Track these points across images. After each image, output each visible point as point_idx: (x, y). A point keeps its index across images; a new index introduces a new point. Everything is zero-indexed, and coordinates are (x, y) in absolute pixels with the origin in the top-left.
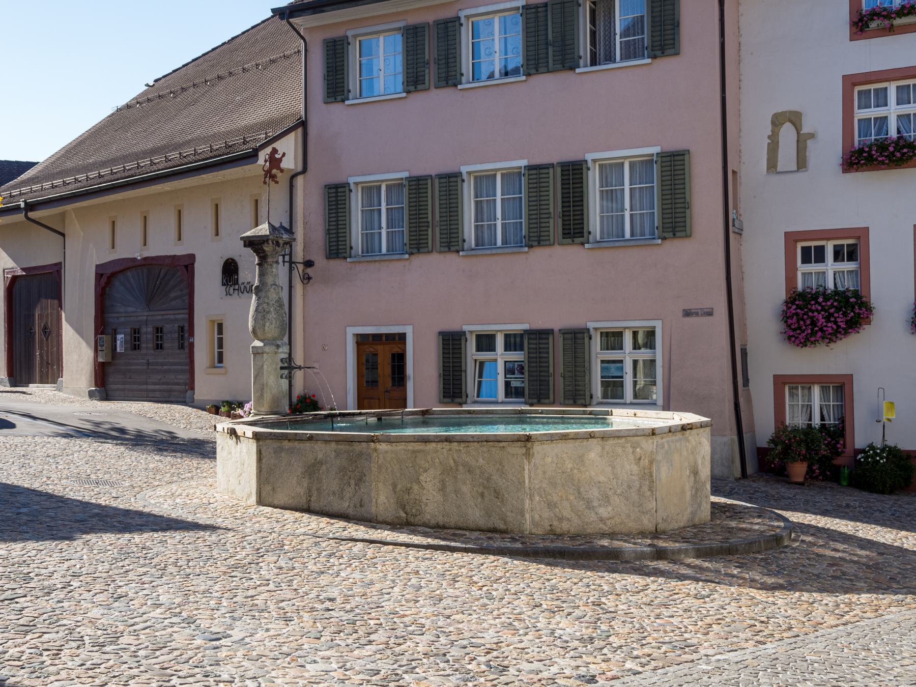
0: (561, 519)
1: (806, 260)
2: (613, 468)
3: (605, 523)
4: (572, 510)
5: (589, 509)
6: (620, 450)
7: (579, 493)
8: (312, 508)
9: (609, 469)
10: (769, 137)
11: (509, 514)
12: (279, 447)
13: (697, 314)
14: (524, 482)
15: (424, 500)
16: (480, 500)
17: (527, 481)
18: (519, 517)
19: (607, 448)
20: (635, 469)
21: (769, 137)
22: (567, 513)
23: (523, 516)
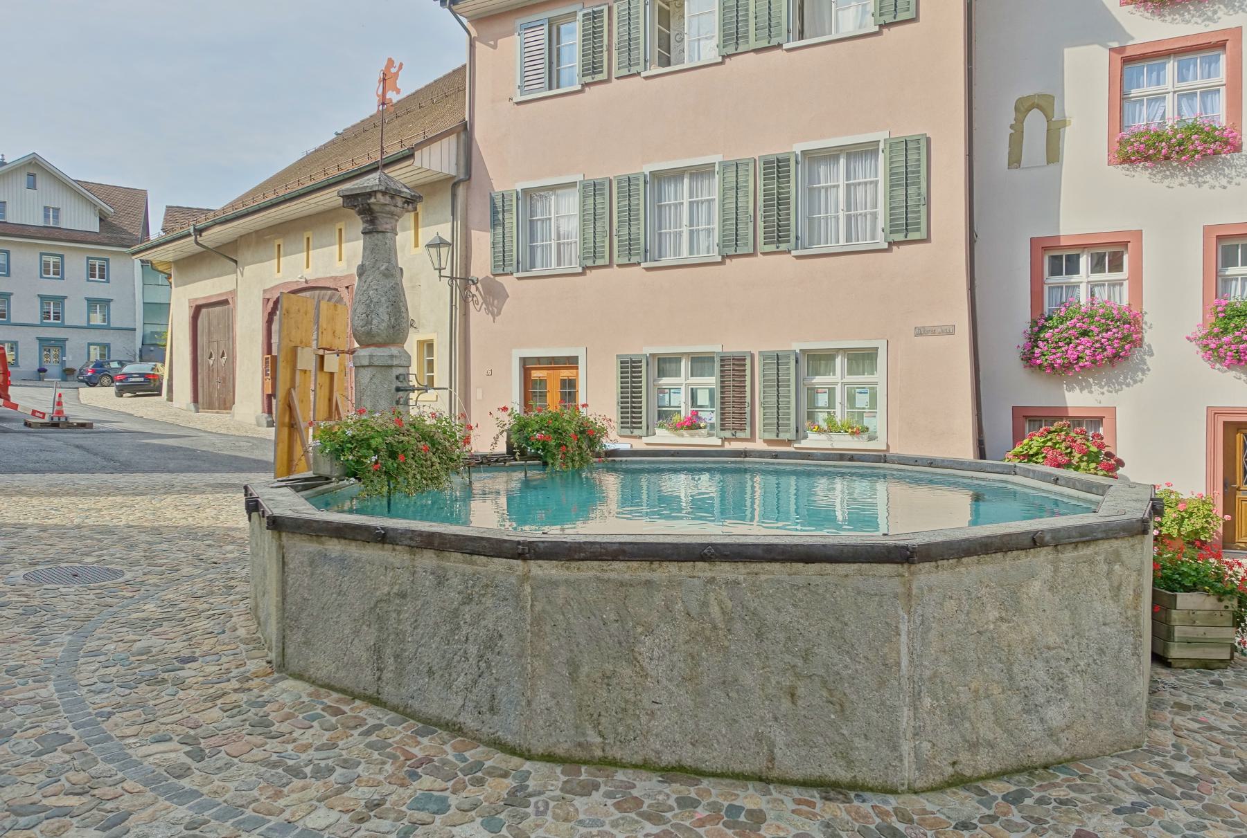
0: (974, 746)
1: (1056, 271)
2: (1074, 612)
3: (1057, 742)
4: (997, 722)
5: (1028, 712)
6: (1085, 569)
7: (1011, 678)
8: (384, 697)
9: (1066, 616)
10: (1012, 127)
11: (859, 742)
12: (319, 553)
13: (934, 333)
14: (898, 664)
15: (646, 703)
16: (786, 704)
17: (905, 662)
18: (885, 752)
19: (1065, 568)
20: (1112, 608)
21: (1012, 127)
22: (986, 730)
23: (895, 748)
